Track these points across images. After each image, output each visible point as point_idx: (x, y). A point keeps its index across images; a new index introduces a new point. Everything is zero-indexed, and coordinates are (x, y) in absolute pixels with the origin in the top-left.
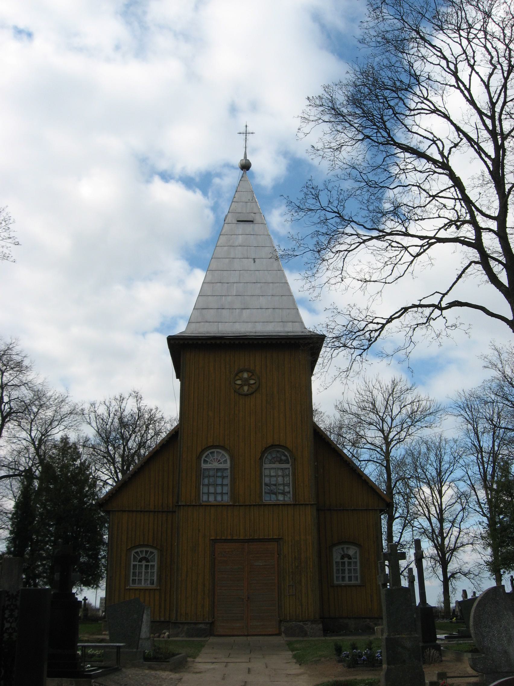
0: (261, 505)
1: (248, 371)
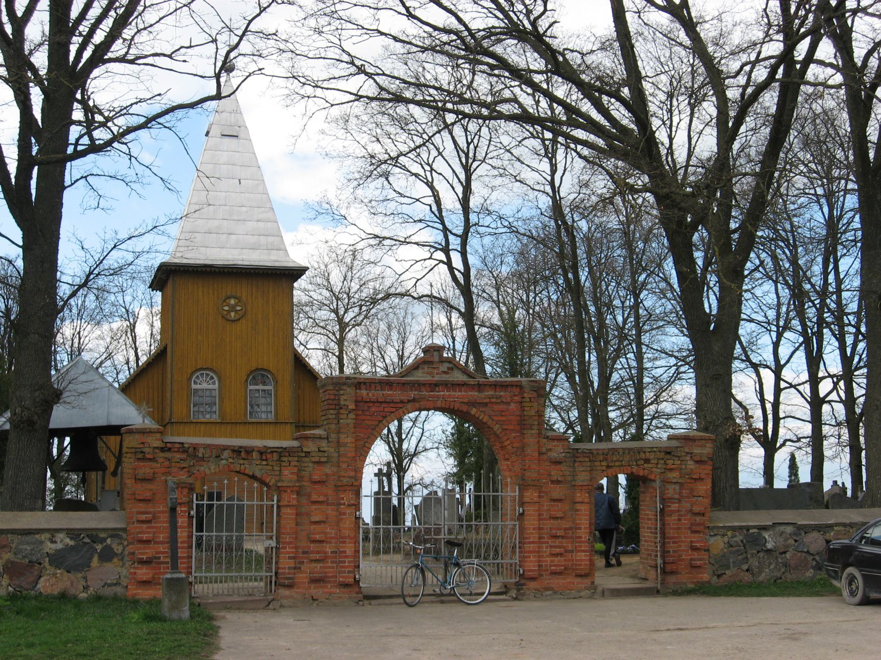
0: (246, 423)
1: (235, 298)
